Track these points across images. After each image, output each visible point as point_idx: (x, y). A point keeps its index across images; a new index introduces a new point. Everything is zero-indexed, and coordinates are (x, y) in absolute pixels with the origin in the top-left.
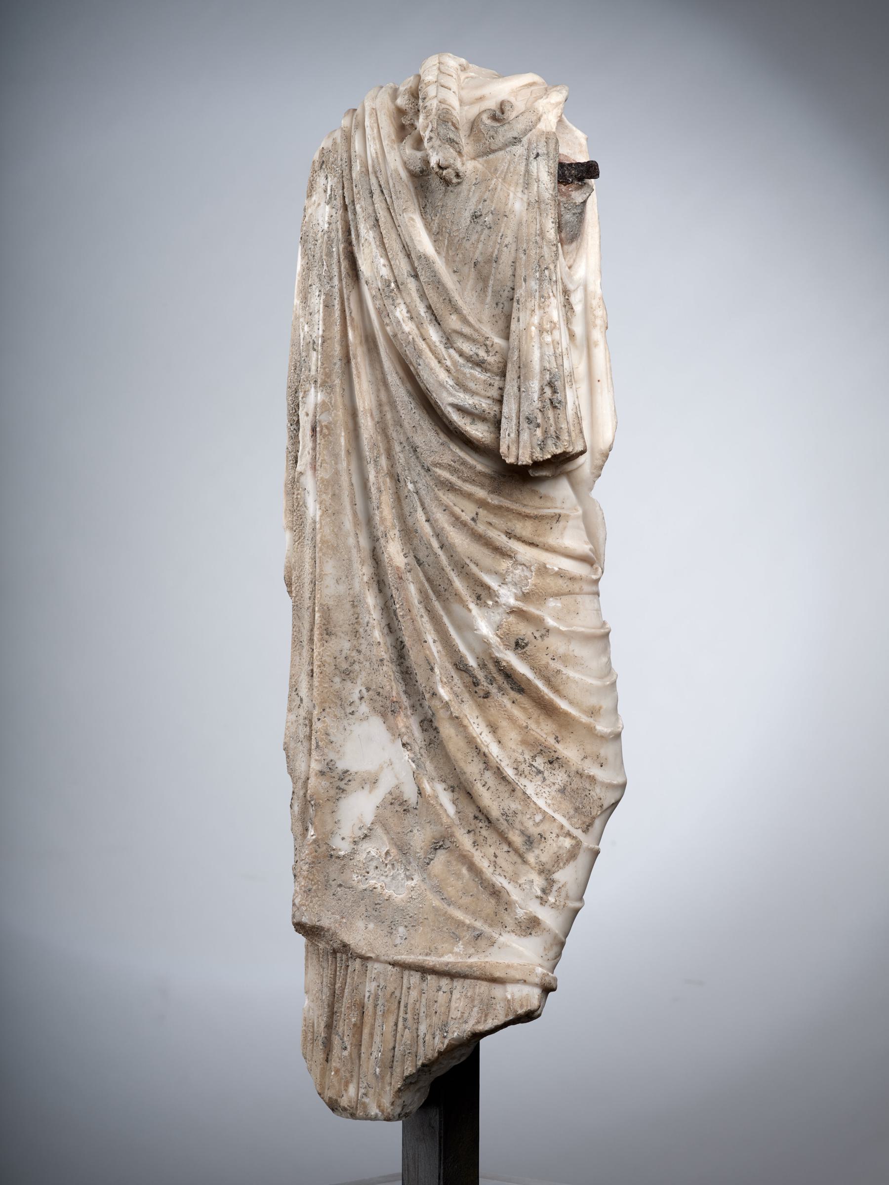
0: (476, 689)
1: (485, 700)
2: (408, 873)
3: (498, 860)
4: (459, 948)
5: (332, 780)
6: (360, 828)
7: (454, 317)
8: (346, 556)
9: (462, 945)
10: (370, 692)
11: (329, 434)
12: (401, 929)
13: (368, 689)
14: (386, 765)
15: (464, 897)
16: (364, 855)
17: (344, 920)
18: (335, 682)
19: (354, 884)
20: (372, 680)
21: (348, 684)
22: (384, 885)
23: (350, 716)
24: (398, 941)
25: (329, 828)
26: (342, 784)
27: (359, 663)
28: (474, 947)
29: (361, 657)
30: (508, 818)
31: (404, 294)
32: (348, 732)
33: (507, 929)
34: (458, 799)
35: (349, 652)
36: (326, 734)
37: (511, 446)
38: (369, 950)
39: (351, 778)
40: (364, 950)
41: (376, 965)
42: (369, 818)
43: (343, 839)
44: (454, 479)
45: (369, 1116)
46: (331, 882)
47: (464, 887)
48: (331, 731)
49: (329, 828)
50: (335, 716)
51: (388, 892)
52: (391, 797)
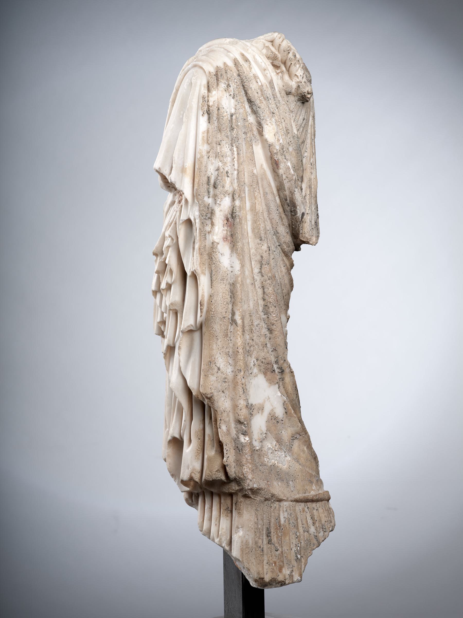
6: (261, 434)
9: (315, 485)
10: (258, 362)
13: (257, 360)
17: (269, 483)
20: (259, 355)
27: (253, 346)
35: (249, 341)
40: (282, 497)
41: (285, 503)
42: (264, 429)
45: (294, 582)
52: (270, 416)
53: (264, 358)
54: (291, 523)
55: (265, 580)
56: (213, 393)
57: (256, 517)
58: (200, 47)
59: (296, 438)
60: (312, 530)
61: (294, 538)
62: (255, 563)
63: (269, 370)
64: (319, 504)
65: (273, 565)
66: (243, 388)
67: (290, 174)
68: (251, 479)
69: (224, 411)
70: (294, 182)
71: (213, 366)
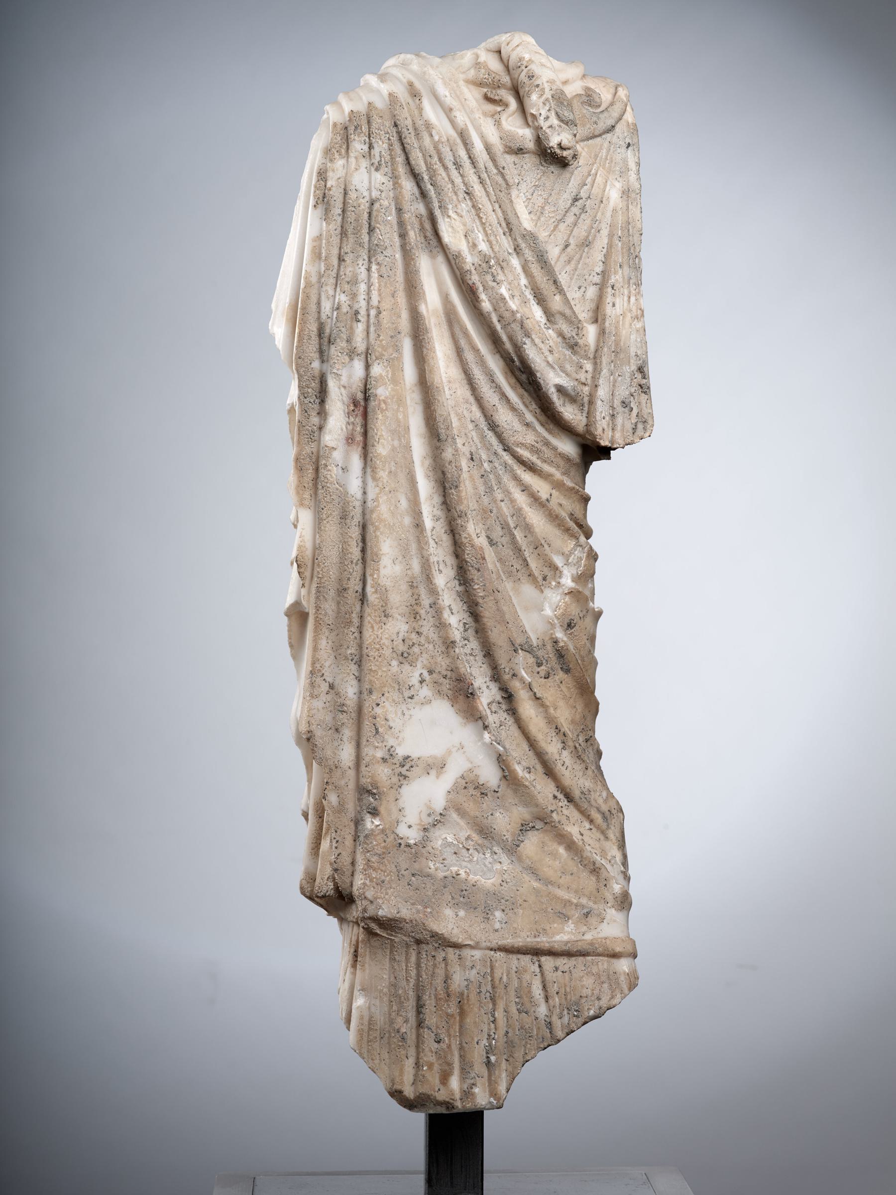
0: (539, 669)
1: (546, 680)
2: (495, 857)
3: (584, 838)
4: (570, 926)
5: (394, 766)
6: (429, 815)
7: (558, 298)
8: (403, 535)
10: (434, 675)
11: (386, 409)
12: (498, 914)
13: (431, 672)
14: (456, 749)
15: (563, 877)
16: (440, 842)
17: (429, 910)
18: (392, 665)
19: (432, 871)
21: (406, 667)
22: (468, 871)
23: (410, 700)
24: (497, 926)
25: (394, 817)
26: (403, 771)
28: (585, 925)
29: (422, 640)
30: (586, 796)
31: (506, 271)
32: (407, 716)
33: (609, 905)
34: (535, 780)
36: (386, 719)
37: (631, 431)
38: (465, 938)
39: (413, 763)
40: (461, 939)
42: (439, 803)
43: (410, 827)
44: (534, 459)
46: (403, 872)
47: (562, 867)
48: (390, 717)
49: (394, 817)
50: (394, 700)
51: (472, 878)
53: (450, 669)
54: (484, 993)
55: (405, 1096)
56: (312, 731)
57: (393, 973)
58: (387, 59)
59: (534, 827)
60: (542, 1010)
61: (486, 1022)
62: (387, 1061)
63: (461, 692)
64: (575, 960)
65: (424, 1069)
66: (374, 725)
67: (507, 310)
68: (372, 900)
69: (336, 767)
70: (520, 326)
71: (317, 680)
